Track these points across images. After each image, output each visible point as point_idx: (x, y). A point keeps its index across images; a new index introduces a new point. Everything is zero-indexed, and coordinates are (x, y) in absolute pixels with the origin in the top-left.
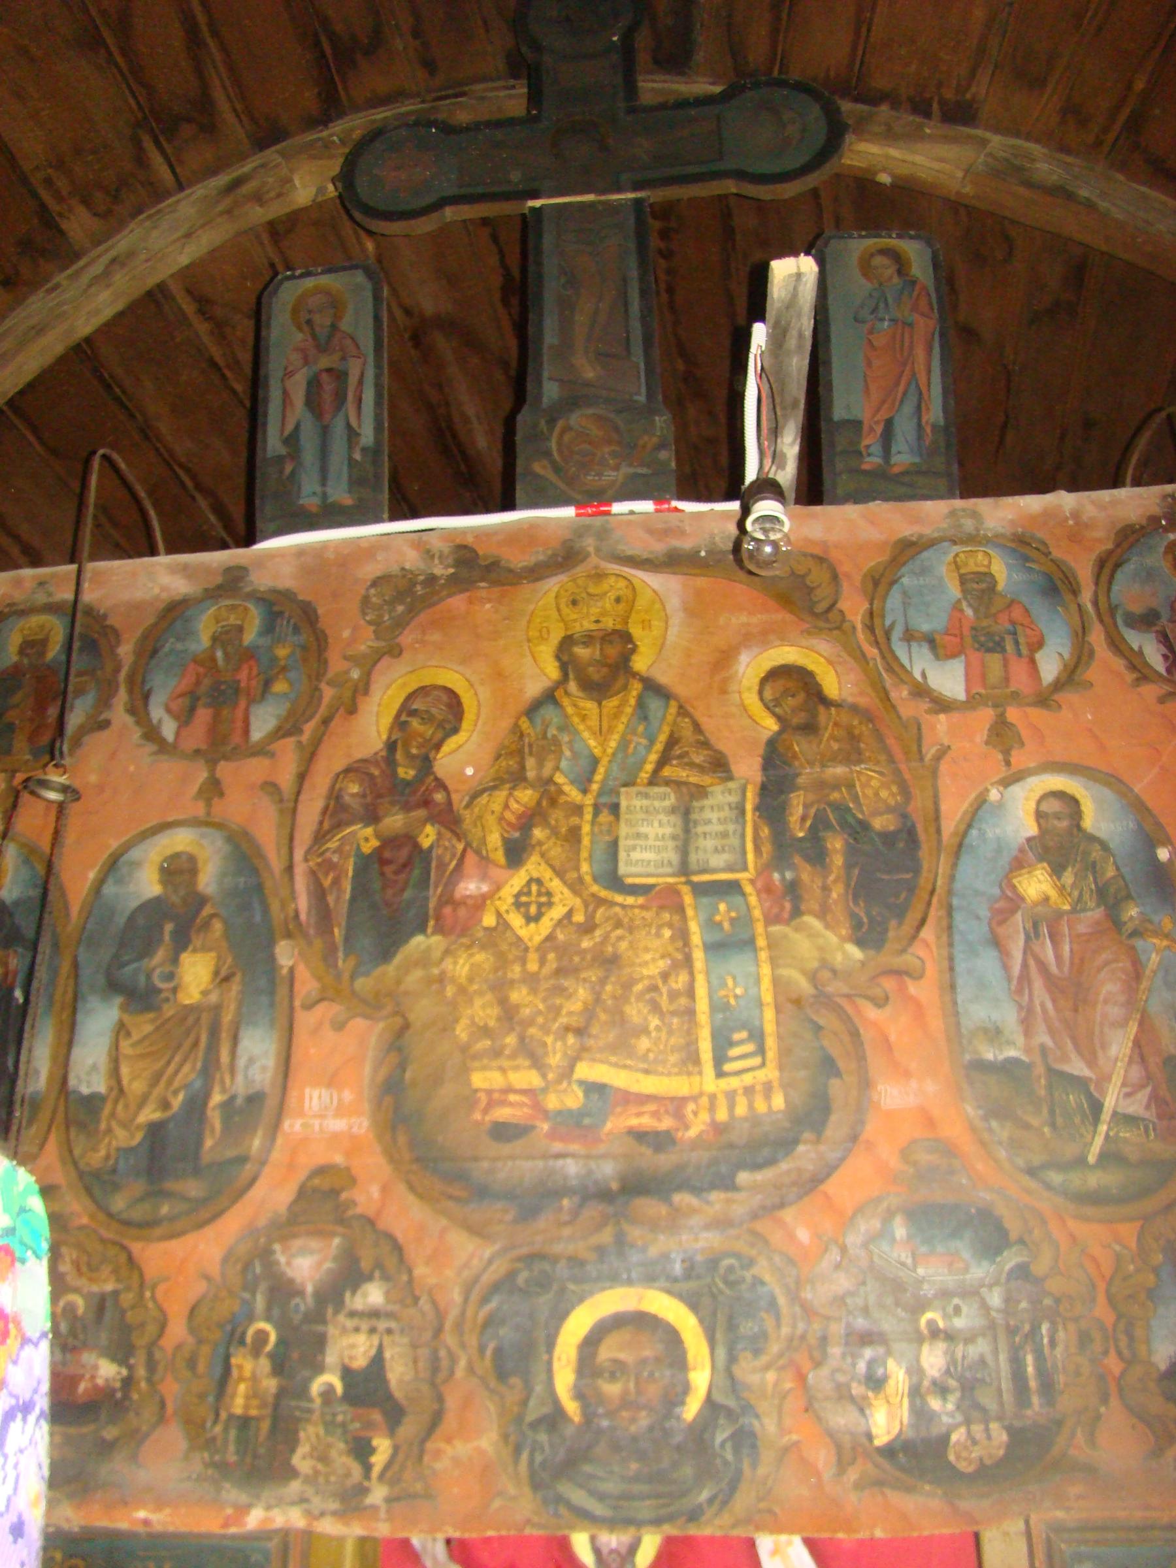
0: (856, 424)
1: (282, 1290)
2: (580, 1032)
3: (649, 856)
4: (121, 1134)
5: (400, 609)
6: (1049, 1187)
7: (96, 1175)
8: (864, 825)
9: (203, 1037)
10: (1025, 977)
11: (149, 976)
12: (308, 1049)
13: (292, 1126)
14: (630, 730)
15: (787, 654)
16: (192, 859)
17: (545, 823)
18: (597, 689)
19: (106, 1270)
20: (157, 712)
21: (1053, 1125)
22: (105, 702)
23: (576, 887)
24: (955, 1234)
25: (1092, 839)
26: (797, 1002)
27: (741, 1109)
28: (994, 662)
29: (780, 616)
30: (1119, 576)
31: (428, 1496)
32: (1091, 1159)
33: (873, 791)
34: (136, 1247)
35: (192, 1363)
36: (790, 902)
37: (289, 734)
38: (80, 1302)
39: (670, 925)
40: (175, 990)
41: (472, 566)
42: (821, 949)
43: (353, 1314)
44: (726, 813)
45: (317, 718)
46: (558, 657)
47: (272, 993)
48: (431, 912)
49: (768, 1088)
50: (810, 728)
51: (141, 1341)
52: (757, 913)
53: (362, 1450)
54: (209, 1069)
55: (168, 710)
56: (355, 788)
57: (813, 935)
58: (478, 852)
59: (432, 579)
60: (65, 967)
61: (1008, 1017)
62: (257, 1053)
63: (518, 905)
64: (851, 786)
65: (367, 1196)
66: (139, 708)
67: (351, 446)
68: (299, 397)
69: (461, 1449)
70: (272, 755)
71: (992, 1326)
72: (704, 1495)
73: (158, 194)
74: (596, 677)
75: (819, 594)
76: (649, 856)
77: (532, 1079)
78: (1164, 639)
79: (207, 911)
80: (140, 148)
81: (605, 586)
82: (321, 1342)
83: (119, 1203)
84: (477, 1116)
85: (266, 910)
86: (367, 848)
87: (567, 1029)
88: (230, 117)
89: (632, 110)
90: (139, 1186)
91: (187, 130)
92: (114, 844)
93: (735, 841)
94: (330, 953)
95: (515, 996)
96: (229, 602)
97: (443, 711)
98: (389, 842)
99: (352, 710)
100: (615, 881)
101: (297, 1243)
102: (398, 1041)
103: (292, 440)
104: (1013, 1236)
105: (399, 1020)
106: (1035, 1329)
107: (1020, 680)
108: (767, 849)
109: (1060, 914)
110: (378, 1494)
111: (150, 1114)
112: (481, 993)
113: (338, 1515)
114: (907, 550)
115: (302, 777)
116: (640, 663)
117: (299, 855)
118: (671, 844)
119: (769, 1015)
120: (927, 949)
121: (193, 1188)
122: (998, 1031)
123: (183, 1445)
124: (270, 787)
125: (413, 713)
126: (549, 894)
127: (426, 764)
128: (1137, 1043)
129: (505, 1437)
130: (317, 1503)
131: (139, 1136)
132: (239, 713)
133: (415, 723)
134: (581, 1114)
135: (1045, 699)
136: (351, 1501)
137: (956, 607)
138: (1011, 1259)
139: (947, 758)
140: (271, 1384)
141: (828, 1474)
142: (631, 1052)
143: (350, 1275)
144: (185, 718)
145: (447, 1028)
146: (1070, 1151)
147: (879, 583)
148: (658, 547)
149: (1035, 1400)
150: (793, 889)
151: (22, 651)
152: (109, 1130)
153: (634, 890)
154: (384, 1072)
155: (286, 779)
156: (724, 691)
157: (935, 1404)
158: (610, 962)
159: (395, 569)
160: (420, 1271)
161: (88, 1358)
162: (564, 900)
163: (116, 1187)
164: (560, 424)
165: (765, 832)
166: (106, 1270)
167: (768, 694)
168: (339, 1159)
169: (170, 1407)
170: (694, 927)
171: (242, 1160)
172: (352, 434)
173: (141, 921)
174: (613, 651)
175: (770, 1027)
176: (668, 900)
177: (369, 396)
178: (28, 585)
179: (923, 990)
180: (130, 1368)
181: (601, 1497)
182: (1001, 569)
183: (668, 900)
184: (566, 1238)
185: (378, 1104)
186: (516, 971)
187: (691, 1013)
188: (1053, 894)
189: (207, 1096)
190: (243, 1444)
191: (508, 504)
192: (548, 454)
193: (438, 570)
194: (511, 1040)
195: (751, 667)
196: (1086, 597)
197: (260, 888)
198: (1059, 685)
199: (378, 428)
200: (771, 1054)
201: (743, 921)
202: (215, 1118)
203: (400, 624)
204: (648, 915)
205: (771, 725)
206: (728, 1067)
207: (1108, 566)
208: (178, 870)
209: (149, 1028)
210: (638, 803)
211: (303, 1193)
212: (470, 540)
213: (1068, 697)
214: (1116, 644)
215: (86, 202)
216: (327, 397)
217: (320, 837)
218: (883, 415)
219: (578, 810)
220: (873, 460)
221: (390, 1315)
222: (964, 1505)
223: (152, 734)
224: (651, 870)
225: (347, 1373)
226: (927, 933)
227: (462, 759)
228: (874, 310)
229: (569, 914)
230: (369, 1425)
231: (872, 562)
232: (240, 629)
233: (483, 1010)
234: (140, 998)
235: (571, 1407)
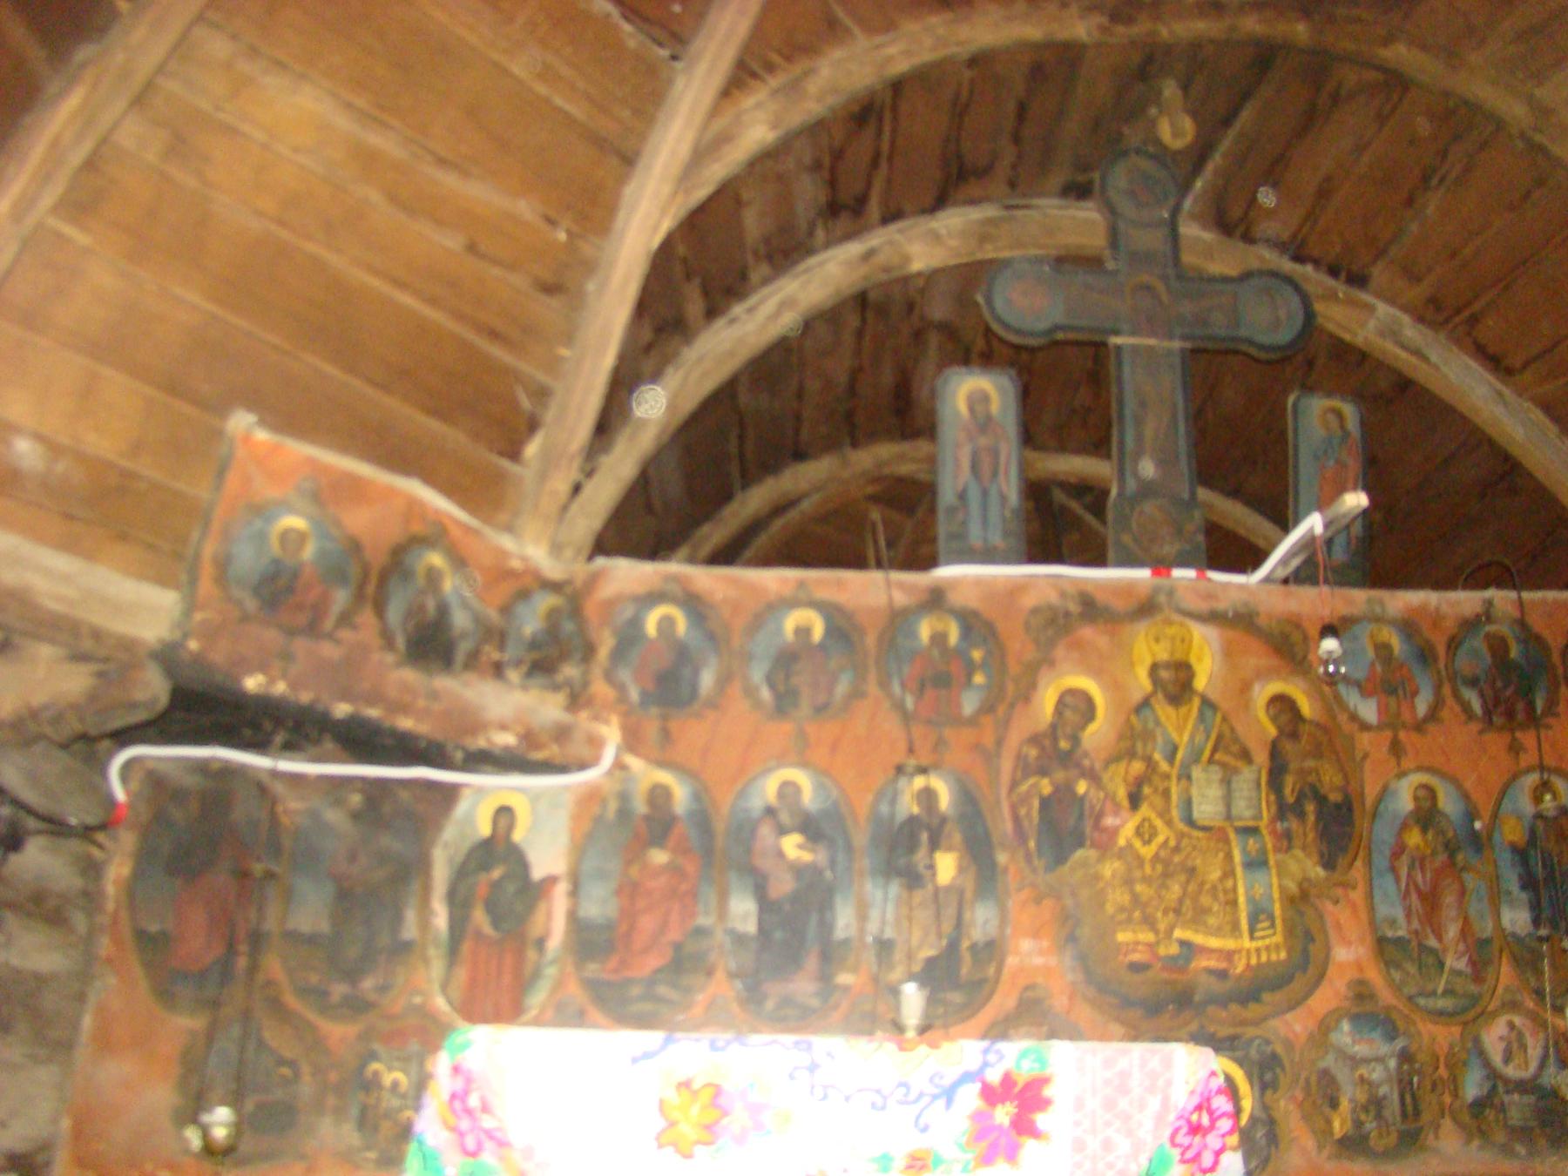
10: (1407, 892)
13: (1012, 961)
14: (1195, 728)
24: (1373, 1029)
27: (1264, 958)
28: (1392, 701)
29: (1274, 661)
32: (1440, 991)
33: (1330, 779)
36: (1286, 840)
41: (1090, 608)
48: (441, 873)
49: (1277, 947)
50: (1294, 735)
59: (1067, 614)
61: (1399, 914)
68: (966, 464)
78: (1482, 695)
84: (1121, 958)
94: (1028, 857)
95: (1139, 888)
100: (1190, 822)
103: (962, 496)
108: (1274, 808)
116: (1200, 683)
120: (1358, 871)
127: (1075, 740)
128: (1462, 930)
135: (1419, 727)
137: (1373, 664)
138: (1400, 1043)
139: (1368, 761)
141: (1314, 1154)
146: (1430, 987)
148: (1202, 606)
150: (1288, 835)
155: (989, 740)
164: (1138, 509)
165: (1272, 797)
172: (1003, 499)
179: (1357, 895)
182: (1396, 643)
188: (1422, 844)
191: (1099, 561)
194: (1137, 914)
196: (1441, 665)
198: (1426, 719)
201: (1263, 851)
202: (967, 958)
203: (1052, 643)
205: (1272, 731)
206: (1258, 934)
207: (1454, 644)
212: (1090, 588)
213: (1431, 727)
217: (1014, 784)
219: (1167, 777)
226: (1358, 863)
227: (1098, 733)
228: (1326, 452)
229: (1166, 842)
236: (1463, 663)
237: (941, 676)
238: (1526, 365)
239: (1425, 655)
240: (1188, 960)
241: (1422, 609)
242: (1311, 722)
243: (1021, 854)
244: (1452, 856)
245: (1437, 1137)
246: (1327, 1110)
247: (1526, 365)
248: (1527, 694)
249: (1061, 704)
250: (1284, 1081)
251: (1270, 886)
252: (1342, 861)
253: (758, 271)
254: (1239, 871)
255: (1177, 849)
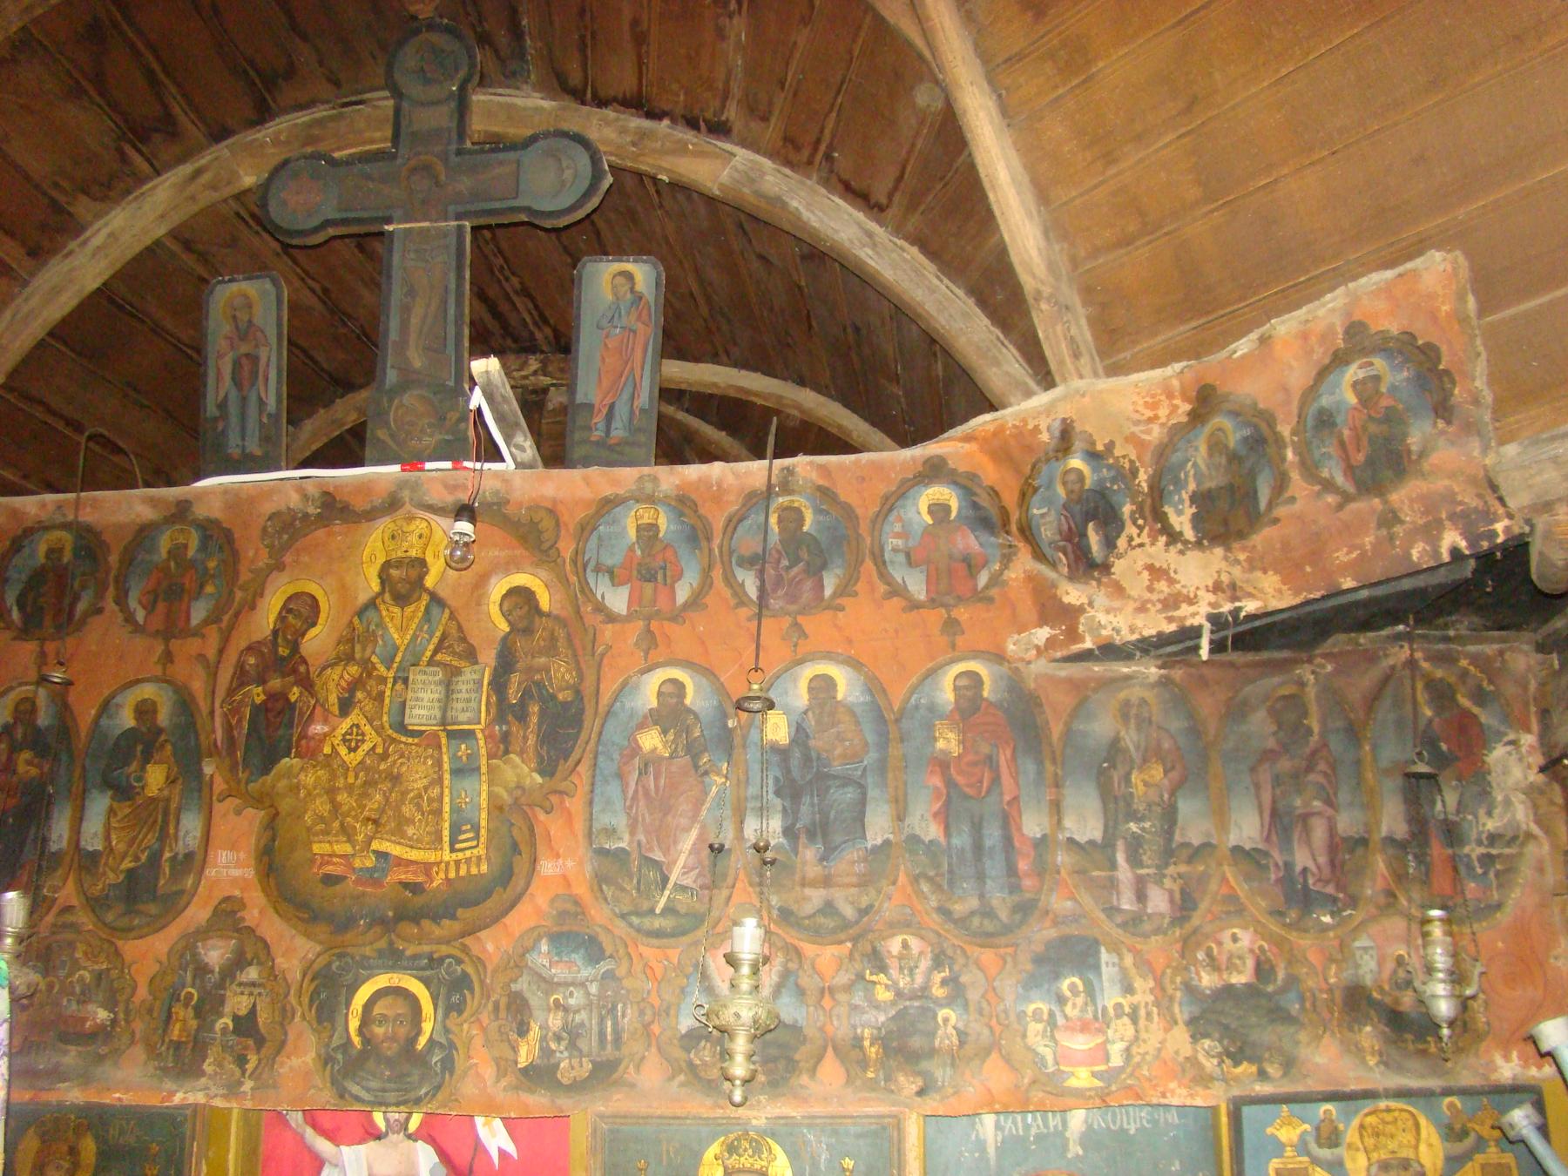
0: (590, 407)
1: (202, 970)
2: (375, 822)
3: (422, 712)
4: (111, 875)
5: (285, 537)
6: (631, 925)
7: (96, 899)
8: (553, 697)
9: (159, 818)
11: (128, 777)
12: (221, 828)
13: (210, 872)
15: (521, 579)
16: (154, 703)
17: (364, 689)
18: (402, 600)
19: (102, 957)
20: (133, 603)
21: (638, 890)
22: (100, 594)
23: (379, 731)
25: (689, 711)
26: (500, 808)
28: (648, 588)
30: (740, 530)
31: (275, 1087)
32: (658, 911)
33: (561, 673)
34: (120, 943)
35: (150, 1011)
36: (503, 745)
37: (214, 622)
38: (87, 975)
39: (432, 756)
40: (143, 788)
42: (518, 776)
43: (240, 984)
44: (471, 686)
45: (231, 612)
46: (380, 577)
47: (200, 790)
50: (528, 631)
51: (122, 998)
52: (483, 751)
53: (241, 1061)
54: (163, 836)
55: (140, 602)
56: (252, 661)
57: (515, 767)
58: (323, 706)
59: (306, 515)
60: (78, 772)
61: (621, 822)
62: (190, 827)
63: (344, 740)
64: (548, 671)
65: (251, 916)
66: (121, 601)
67: (261, 413)
69: (295, 1062)
70: (203, 636)
71: (590, 1004)
72: (423, 1091)
73: (141, 180)
74: (403, 591)
75: (545, 536)
76: (422, 712)
77: (347, 849)
79: (163, 738)
80: (122, 154)
81: (412, 527)
82: (222, 1000)
83: (110, 917)
85: (197, 738)
86: (258, 700)
87: (368, 819)
88: (190, 126)
89: (459, 153)
90: (121, 907)
91: (157, 138)
92: (106, 693)
93: (473, 705)
94: (234, 768)
96: (178, 527)
97: (303, 610)
98: (272, 696)
99: (253, 607)
100: (402, 728)
101: (210, 942)
102: (271, 824)
103: (223, 406)
104: (607, 953)
105: (273, 811)
106: (614, 1007)
107: (663, 603)
108: (493, 711)
109: (662, 758)
110: (248, 1085)
111: (127, 864)
112: (319, 795)
113: (224, 1096)
114: (608, 505)
115: (221, 651)
116: (429, 582)
117: (217, 705)
118: (437, 704)
119: (484, 815)
121: (153, 909)
122: (614, 831)
123: (144, 1057)
124: (201, 657)
125: (290, 611)
126: (363, 734)
127: (295, 647)
129: (319, 1056)
130: (214, 1090)
131: (122, 877)
132: (184, 607)
133: (290, 618)
134: (374, 869)
135: (677, 616)
136: (233, 1090)
137: (631, 549)
138: (604, 966)
140: (193, 1024)
142: (403, 834)
143: (239, 962)
144: (150, 608)
145: (300, 817)
146: (646, 906)
147: (586, 529)
149: (609, 1047)
151: (47, 556)
152: (104, 874)
153: (413, 734)
154: (263, 842)
155: (211, 654)
156: (479, 604)
157: (553, 1046)
158: (396, 779)
159: (283, 508)
160: (279, 960)
161: (91, 1007)
162: (372, 739)
163: (109, 907)
166: (102, 957)
167: (505, 608)
168: (237, 893)
169: (138, 1036)
170: (445, 758)
171: (182, 892)
172: (262, 403)
173: (123, 743)
174: (414, 574)
175: (483, 823)
176: (432, 741)
177: (273, 375)
178: (51, 508)
180: (115, 1013)
181: (368, 1090)
183: (432, 741)
184: (367, 945)
185: (259, 859)
186: (340, 783)
187: (439, 812)
188: (660, 746)
189: (161, 852)
190: (177, 1057)
192: (387, 423)
193: (312, 510)
194: (336, 824)
195: (499, 588)
196: (716, 542)
197: (194, 724)
198: (687, 606)
199: (279, 401)
200: (482, 840)
203: (285, 548)
204: (420, 750)
205: (504, 627)
206: (458, 846)
207: (734, 523)
208: (145, 711)
209: (127, 811)
210: (420, 677)
211: (216, 912)
214: (729, 579)
215: (86, 193)
216: (246, 374)
217: (231, 692)
218: (608, 401)
219: (384, 680)
220: (598, 434)
221: (260, 985)
222: (559, 1102)
223: (129, 618)
224: (424, 721)
225: (236, 1018)
227: (318, 641)
229: (374, 747)
230: (246, 1048)
231: (581, 515)
232: (186, 546)
233: (321, 806)
234: (123, 792)
235: (356, 1040)
236: (748, 541)
237: (171, 592)
238: (890, 196)
239: (696, 535)
240: (385, 872)
241: (704, 481)
242: (548, 615)
243: (227, 761)
244: (695, 757)
245: (638, 1068)
246: (513, 1036)
247: (890, 196)
248: (816, 571)
249: (286, 609)
250: (472, 1004)
251: (479, 794)
252: (563, 767)
253: (82, 207)
254: (447, 776)
255: (384, 756)
